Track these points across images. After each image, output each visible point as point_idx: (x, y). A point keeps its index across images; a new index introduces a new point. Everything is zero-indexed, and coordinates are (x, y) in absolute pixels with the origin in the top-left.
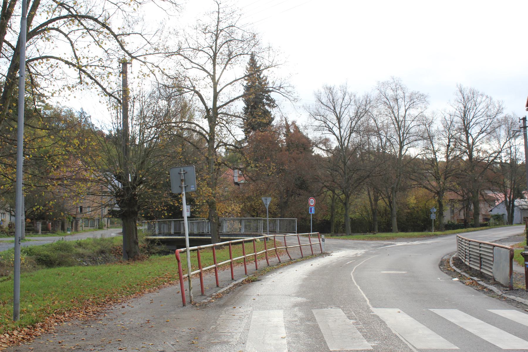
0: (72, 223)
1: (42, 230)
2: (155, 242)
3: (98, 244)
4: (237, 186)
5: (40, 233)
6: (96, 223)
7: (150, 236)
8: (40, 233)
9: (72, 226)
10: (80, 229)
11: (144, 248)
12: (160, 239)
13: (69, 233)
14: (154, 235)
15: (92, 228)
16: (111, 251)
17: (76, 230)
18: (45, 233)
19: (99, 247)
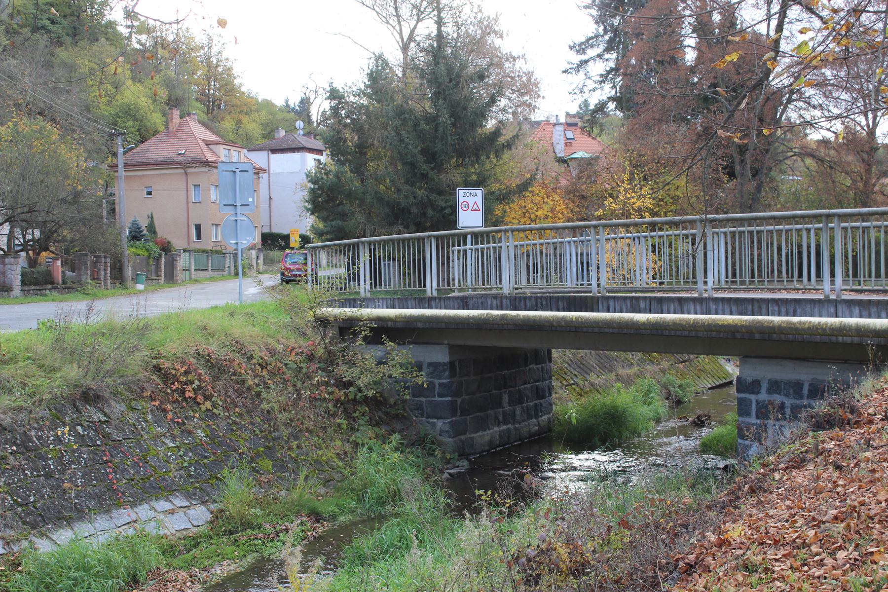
0: (157, 260)
1: (23, 283)
2: (355, 334)
3: (72, 355)
4: (562, 167)
5: (162, 281)
6: (229, 262)
7: (331, 304)
8: (162, 281)
9: (158, 270)
10: (180, 275)
11: (310, 358)
12: (379, 319)
13: (140, 287)
14: (352, 302)
15: (217, 274)
16: (135, 392)
17: (171, 278)
18: (39, 293)
19: (73, 372)
